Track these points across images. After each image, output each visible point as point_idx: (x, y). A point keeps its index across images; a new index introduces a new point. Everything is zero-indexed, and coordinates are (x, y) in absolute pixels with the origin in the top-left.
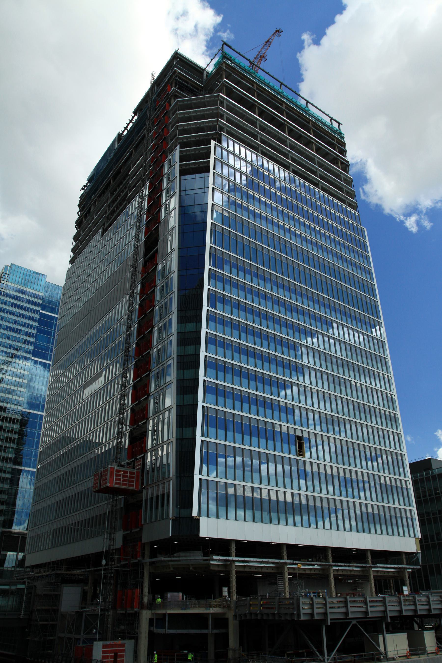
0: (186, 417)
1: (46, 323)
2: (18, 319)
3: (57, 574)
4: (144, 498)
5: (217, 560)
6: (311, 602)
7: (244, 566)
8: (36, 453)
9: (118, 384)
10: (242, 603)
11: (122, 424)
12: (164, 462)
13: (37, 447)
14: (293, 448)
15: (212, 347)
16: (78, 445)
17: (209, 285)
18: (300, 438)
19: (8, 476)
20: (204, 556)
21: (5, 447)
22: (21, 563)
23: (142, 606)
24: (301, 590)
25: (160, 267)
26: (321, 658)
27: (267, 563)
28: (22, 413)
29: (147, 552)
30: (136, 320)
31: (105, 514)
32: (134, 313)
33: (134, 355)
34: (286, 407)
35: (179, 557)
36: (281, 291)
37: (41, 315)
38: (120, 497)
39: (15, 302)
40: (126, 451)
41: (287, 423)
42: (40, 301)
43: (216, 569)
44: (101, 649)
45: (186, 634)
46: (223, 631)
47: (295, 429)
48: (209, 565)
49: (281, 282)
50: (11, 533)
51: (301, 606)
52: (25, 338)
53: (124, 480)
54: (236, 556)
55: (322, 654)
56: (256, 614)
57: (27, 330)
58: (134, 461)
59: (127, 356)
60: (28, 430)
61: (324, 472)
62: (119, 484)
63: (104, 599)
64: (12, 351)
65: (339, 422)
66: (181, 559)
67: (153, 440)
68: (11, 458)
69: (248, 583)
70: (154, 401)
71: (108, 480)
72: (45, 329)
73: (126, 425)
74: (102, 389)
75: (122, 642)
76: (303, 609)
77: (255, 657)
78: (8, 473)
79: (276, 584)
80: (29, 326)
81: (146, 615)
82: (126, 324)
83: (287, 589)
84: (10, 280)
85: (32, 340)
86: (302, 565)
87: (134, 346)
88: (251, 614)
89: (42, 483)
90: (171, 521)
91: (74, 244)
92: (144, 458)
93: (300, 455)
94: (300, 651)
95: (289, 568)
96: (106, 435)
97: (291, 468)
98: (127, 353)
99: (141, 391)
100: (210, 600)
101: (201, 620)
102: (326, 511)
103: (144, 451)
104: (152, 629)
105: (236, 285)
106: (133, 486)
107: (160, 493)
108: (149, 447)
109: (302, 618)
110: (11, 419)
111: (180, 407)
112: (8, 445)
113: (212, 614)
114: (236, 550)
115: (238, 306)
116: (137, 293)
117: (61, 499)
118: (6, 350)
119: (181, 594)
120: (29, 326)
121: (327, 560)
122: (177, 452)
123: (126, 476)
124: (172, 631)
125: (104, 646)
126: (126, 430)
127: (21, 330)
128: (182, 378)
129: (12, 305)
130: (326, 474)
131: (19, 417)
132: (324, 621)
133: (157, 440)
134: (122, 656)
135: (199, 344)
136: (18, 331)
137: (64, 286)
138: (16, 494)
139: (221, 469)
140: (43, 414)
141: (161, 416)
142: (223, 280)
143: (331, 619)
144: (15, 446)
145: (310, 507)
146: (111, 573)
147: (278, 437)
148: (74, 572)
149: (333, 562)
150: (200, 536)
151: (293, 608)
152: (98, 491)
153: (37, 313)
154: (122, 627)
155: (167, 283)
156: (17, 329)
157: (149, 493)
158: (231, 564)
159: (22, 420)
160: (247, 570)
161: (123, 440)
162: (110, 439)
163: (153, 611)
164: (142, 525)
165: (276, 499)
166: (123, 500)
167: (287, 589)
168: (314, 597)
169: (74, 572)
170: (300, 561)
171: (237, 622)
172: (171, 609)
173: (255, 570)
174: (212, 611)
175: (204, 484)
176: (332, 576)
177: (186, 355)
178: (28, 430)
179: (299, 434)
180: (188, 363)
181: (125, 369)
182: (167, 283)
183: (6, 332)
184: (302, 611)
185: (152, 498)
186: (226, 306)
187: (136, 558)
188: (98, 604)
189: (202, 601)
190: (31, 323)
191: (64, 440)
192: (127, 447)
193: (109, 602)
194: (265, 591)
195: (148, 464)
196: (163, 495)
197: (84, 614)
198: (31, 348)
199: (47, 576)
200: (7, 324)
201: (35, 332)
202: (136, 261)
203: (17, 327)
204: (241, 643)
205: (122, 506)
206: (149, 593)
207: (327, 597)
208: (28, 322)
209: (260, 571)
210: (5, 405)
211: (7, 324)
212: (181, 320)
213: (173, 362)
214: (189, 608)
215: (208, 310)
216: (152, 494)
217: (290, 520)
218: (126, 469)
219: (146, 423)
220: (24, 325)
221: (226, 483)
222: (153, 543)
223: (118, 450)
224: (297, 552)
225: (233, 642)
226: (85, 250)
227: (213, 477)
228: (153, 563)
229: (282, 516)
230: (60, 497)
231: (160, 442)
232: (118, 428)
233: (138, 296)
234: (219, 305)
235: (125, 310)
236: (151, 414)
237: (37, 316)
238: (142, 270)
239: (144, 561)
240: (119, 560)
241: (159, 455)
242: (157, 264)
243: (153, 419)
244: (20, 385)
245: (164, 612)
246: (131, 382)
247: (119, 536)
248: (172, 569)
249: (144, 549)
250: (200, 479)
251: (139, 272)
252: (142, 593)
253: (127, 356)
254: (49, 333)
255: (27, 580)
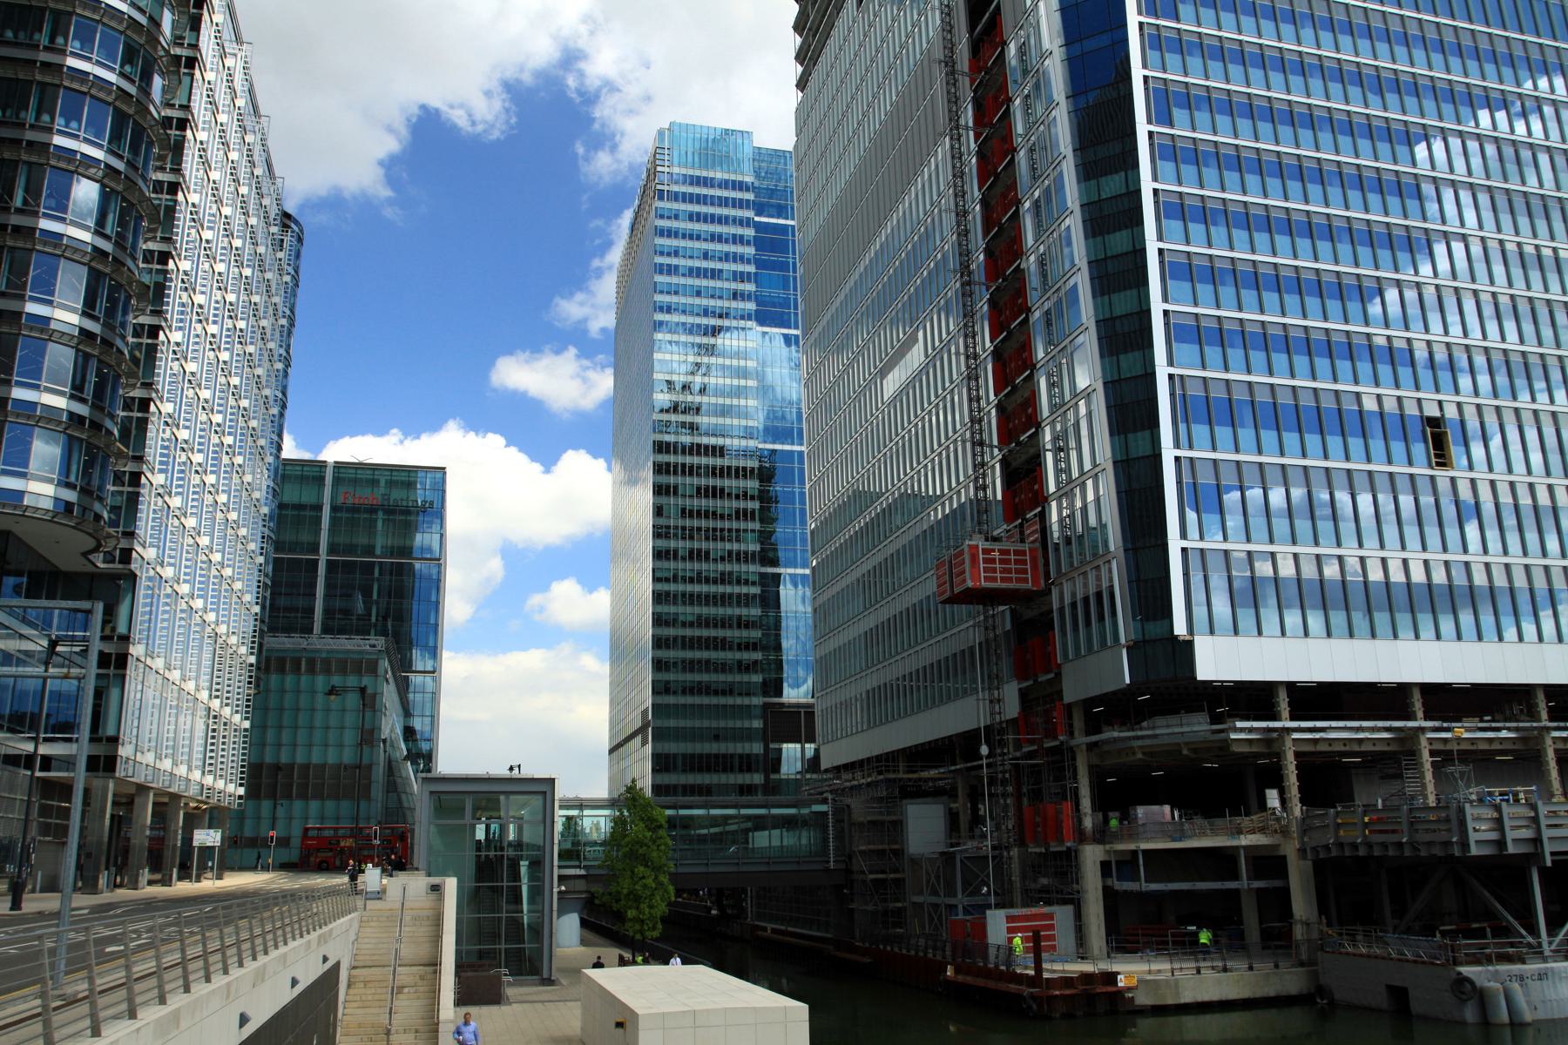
0: (1131, 409)
1: (772, 244)
2: (711, 246)
3: (888, 780)
4: (1055, 606)
5: (1244, 730)
6: (1495, 815)
7: (1316, 741)
8: (803, 534)
9: (957, 353)
10: (1317, 823)
11: (981, 444)
12: (1093, 521)
13: (803, 522)
14: (1419, 449)
15: (1175, 226)
16: (889, 506)
17: (1145, 66)
18: (1434, 422)
19: (755, 590)
20: (1212, 723)
21: (738, 531)
22: (813, 764)
23: (1082, 837)
24: (1468, 787)
25: (1012, 49)
26: (1530, 939)
27: (1373, 730)
28: (759, 455)
29: (1078, 723)
30: (976, 193)
31: (972, 649)
32: (967, 178)
33: (983, 279)
34: (1390, 348)
35: (1154, 728)
36: (1345, 40)
37: (759, 227)
38: (1001, 608)
39: (696, 208)
40: (1000, 508)
41: (1397, 386)
42: (750, 196)
43: (1246, 749)
44: (1004, 925)
45: (1188, 891)
46: (1277, 883)
47: (1419, 400)
48: (1227, 743)
49: (1344, 18)
50: (782, 705)
51: (1470, 825)
52: (733, 286)
53: (1003, 571)
54: (1292, 719)
55: (1533, 930)
56: (1354, 846)
57: (733, 267)
58: (1021, 525)
59: (969, 283)
60: (778, 488)
61: (1511, 500)
62: (994, 579)
63: (998, 827)
64: (713, 322)
65: (1545, 367)
66: (1158, 732)
67: (1058, 471)
68: (754, 553)
69: (1326, 777)
70: (1048, 380)
71: (967, 574)
72: (774, 257)
73: (991, 446)
74: (924, 370)
75: (1046, 910)
76: (1475, 830)
77: (1360, 937)
78: (754, 583)
79: (1399, 776)
80: (736, 258)
81: (1092, 855)
82: (952, 207)
83: (1430, 788)
84: (676, 160)
85: (750, 287)
86: (1464, 731)
87: (982, 257)
88: (1341, 845)
89: (826, 596)
90: (1124, 651)
91: (799, 40)
92: (1043, 517)
93: (1438, 464)
94: (1475, 926)
95: (1431, 741)
96: (948, 472)
97: (1416, 500)
98: (966, 278)
99: (1013, 363)
100: (1238, 820)
101: (1222, 861)
102: (1524, 601)
103: (1042, 500)
104: (1109, 882)
105: (1220, 52)
106: (1026, 580)
107: (1092, 590)
108: (1052, 488)
109: (1474, 851)
110: (737, 469)
111: (1113, 387)
112: (742, 525)
113: (1246, 848)
114: (1290, 704)
115: (1230, 106)
116: (967, 128)
117: (872, 625)
118: (698, 320)
119: (1167, 808)
120: (736, 258)
121: (1533, 715)
122: (1118, 493)
123: (1007, 561)
124: (1154, 887)
125: (1010, 919)
126: (993, 458)
127: (721, 271)
128: (1108, 315)
129: (693, 217)
130: (1536, 507)
131: (752, 463)
132: (1535, 857)
133: (1068, 470)
134: (1052, 938)
135: (1140, 222)
136: (715, 274)
137: (796, 147)
138: (777, 625)
139: (1234, 522)
140: (803, 448)
141: (1071, 415)
142: (1179, 45)
143: (1552, 854)
144: (757, 526)
145: (1476, 592)
146: (1004, 772)
147: (1375, 427)
148: (925, 774)
149: (1551, 719)
150: (1199, 678)
151: (1449, 830)
152: (954, 600)
153: (748, 225)
154: (1044, 881)
155: (1037, 86)
156: (713, 270)
157: (1065, 594)
158: (1281, 739)
159: (761, 468)
160: (1322, 748)
161: (989, 481)
162: (958, 483)
163: (1108, 847)
164: (1059, 666)
165: (1403, 579)
166: (1008, 614)
167: (1430, 788)
168: (1504, 804)
169: (925, 774)
170: (1459, 721)
171: (1310, 863)
172: (1148, 840)
173: (1343, 749)
174: (1245, 840)
175: (1194, 561)
176: (1551, 754)
177: (1113, 257)
178: (778, 488)
179: (1432, 411)
180: (1120, 274)
181: (968, 314)
182: (1037, 86)
183: (690, 281)
184: (1473, 837)
185: (1074, 605)
186: (1196, 114)
187: (1056, 738)
188: (984, 836)
189: (1219, 822)
190: (739, 249)
191: (859, 499)
192: (999, 497)
193: (1008, 831)
194: (1373, 796)
195: (1055, 527)
196: (1099, 595)
197: (958, 857)
198: (751, 306)
199: (869, 785)
200: (690, 263)
201: (751, 269)
202: (950, 47)
203: (711, 265)
204: (1323, 909)
205: (1008, 626)
206: (1094, 810)
207: (1540, 803)
208: (732, 248)
209: (1356, 748)
210: (720, 441)
211: (690, 263)
212: (1088, 171)
213: (1082, 282)
214: (1190, 837)
215: (1151, 134)
216: (1074, 594)
217: (1447, 625)
218: (1004, 546)
219: (1036, 434)
220: (726, 257)
221: (1249, 553)
222: (1089, 703)
223: (980, 507)
224: (1446, 700)
225: (1302, 906)
226: (827, 50)
227: (1214, 543)
228: (1095, 744)
229: (1425, 621)
230: (870, 622)
231: (1075, 474)
232: (974, 455)
233: (971, 134)
234: (1179, 114)
235: (946, 175)
236: (1046, 413)
237: (749, 232)
238: (971, 69)
239: (1073, 743)
240: (1018, 745)
241: (1079, 504)
242: (1004, 44)
243: (1053, 423)
244: (739, 392)
245: (1132, 847)
246: (988, 344)
247: (1011, 696)
248: (1140, 756)
249: (1070, 717)
250: (1184, 550)
251: (963, 74)
252: (1078, 810)
253: (969, 283)
254: (784, 266)
255: (830, 797)
